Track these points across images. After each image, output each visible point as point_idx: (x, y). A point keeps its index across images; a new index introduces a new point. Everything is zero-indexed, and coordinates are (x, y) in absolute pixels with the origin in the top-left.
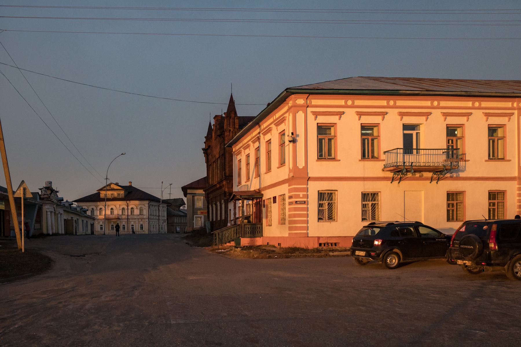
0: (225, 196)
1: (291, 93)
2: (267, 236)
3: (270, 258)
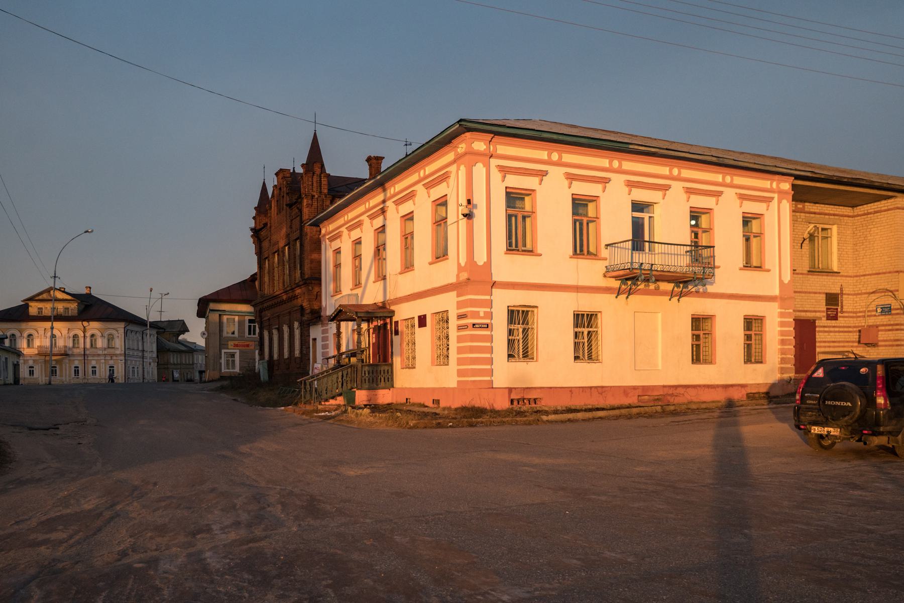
0: (302, 315)
1: (466, 128)
2: (404, 387)
3: (439, 428)
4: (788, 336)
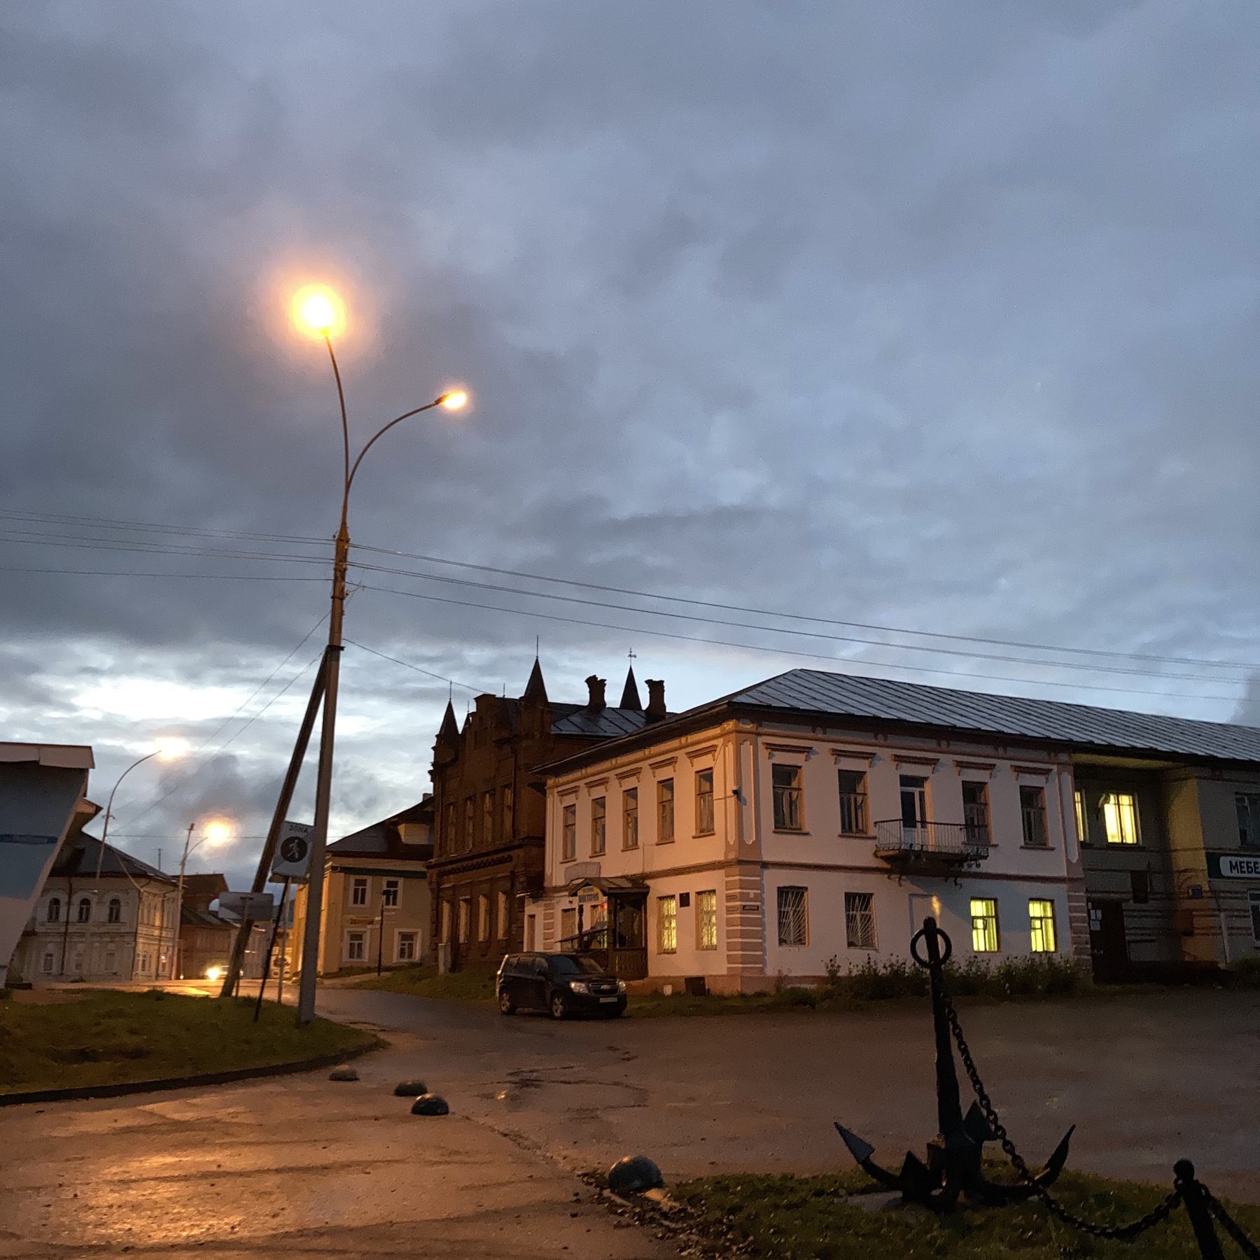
4: (756, 926)
